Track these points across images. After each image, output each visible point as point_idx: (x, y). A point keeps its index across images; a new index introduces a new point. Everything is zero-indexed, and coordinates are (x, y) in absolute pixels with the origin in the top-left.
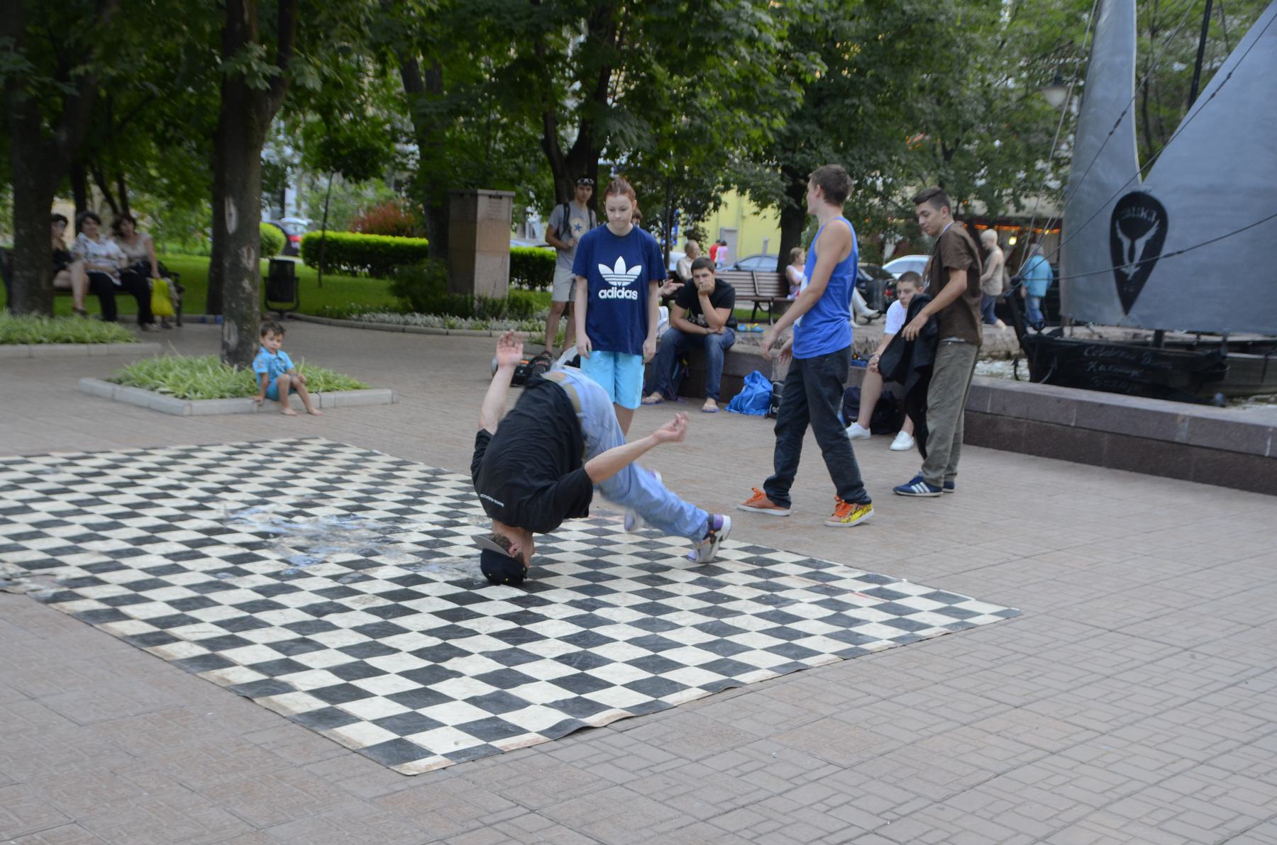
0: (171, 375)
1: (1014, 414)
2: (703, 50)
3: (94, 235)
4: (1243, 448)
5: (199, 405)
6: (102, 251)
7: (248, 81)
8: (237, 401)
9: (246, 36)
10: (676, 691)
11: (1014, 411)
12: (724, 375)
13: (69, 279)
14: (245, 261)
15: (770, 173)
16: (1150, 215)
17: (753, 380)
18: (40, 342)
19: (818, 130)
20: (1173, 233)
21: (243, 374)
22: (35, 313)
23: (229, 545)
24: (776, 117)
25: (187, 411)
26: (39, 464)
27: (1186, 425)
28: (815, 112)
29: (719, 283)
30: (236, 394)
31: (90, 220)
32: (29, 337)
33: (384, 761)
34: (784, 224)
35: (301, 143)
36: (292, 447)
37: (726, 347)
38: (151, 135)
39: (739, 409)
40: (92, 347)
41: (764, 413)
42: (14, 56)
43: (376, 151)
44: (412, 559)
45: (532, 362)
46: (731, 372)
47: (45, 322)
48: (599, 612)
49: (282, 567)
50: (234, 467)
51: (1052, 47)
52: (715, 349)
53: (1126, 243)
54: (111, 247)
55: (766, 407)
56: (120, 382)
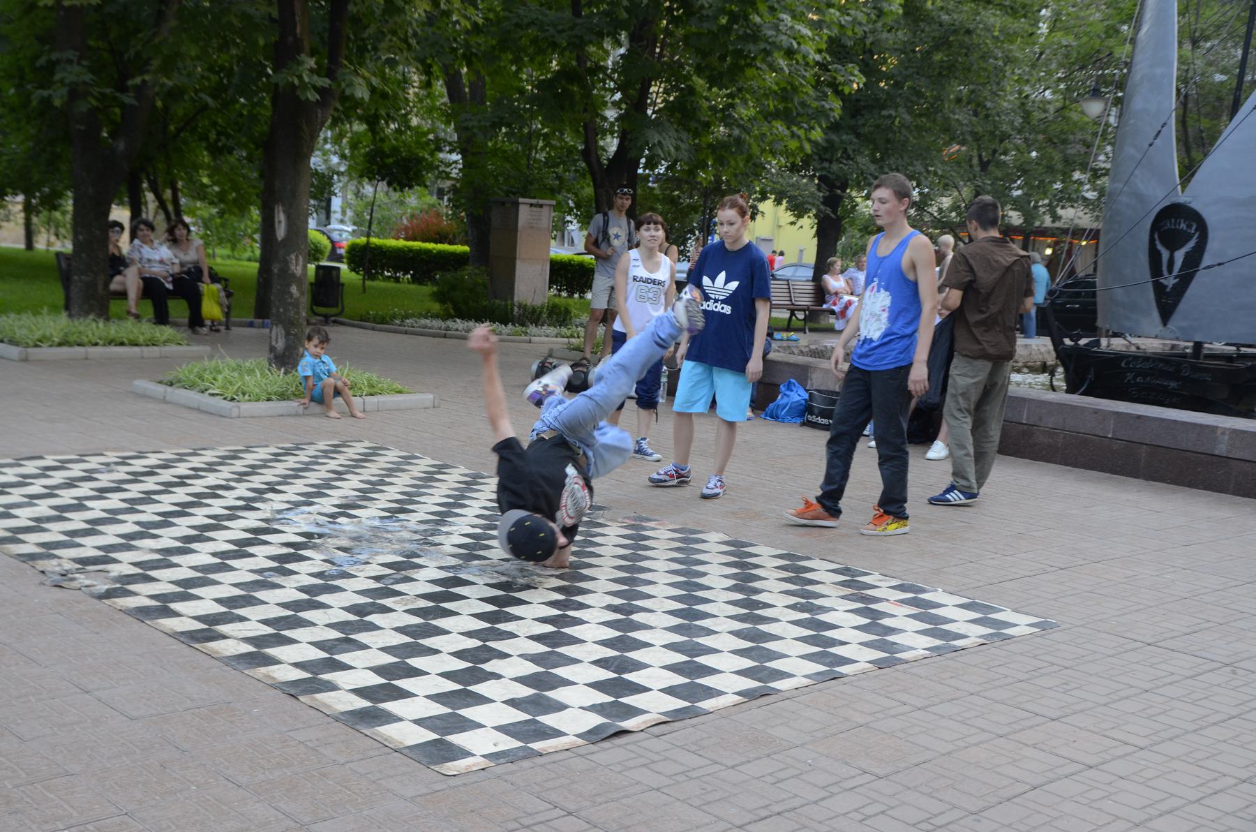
0: (220, 377)
5: (246, 407)
7: (298, 92)
11: (1050, 422)
13: (123, 284)
14: (293, 267)
15: (807, 184)
16: (1189, 226)
17: (789, 389)
18: (96, 344)
20: (1213, 245)
21: (289, 378)
22: (91, 317)
23: (275, 545)
24: (813, 128)
28: (852, 122)
30: (283, 396)
32: (86, 340)
33: (424, 761)
38: (204, 144)
39: (774, 416)
40: (145, 349)
41: (799, 421)
42: (77, 69)
44: (453, 562)
47: (101, 325)
50: (280, 468)
53: (1165, 254)
54: (165, 252)
55: (801, 415)
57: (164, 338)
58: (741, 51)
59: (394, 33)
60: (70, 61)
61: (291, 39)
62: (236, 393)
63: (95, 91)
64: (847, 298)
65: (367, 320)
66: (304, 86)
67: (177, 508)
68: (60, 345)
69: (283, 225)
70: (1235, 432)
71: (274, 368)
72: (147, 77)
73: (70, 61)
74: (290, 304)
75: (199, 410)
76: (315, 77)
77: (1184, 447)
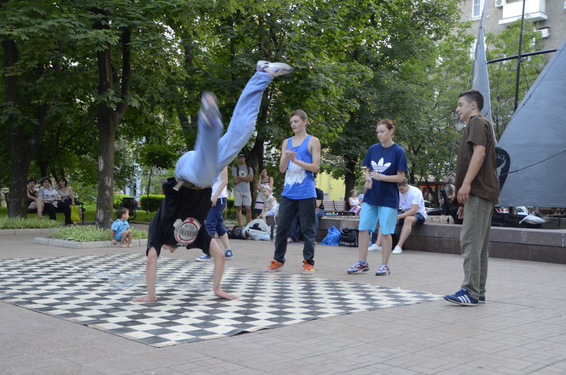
0: (74, 233)
5: (84, 244)
7: (107, 104)
8: (102, 242)
9: (108, 86)
10: (287, 321)
13: (36, 206)
16: (502, 157)
17: (332, 231)
18: (20, 228)
20: (513, 166)
21: (105, 232)
22: (18, 217)
23: (88, 282)
24: (339, 127)
26: (8, 262)
30: (102, 239)
31: (47, 181)
32: (15, 226)
34: (347, 182)
37: (320, 218)
39: (326, 243)
40: (42, 229)
41: (337, 244)
42: (13, 108)
43: (170, 156)
44: (172, 285)
45: (234, 228)
46: (322, 228)
47: (23, 220)
48: (255, 298)
49: (110, 288)
54: (55, 192)
57: (51, 225)
59: (152, 86)
60: (10, 106)
61: (105, 83)
64: (359, 207)
67: (58, 301)
68: (3, 228)
69: (102, 164)
70: (529, 232)
71: (98, 229)
72: (40, 101)
73: (10, 106)
74: (106, 199)
76: (115, 98)
77: (508, 241)
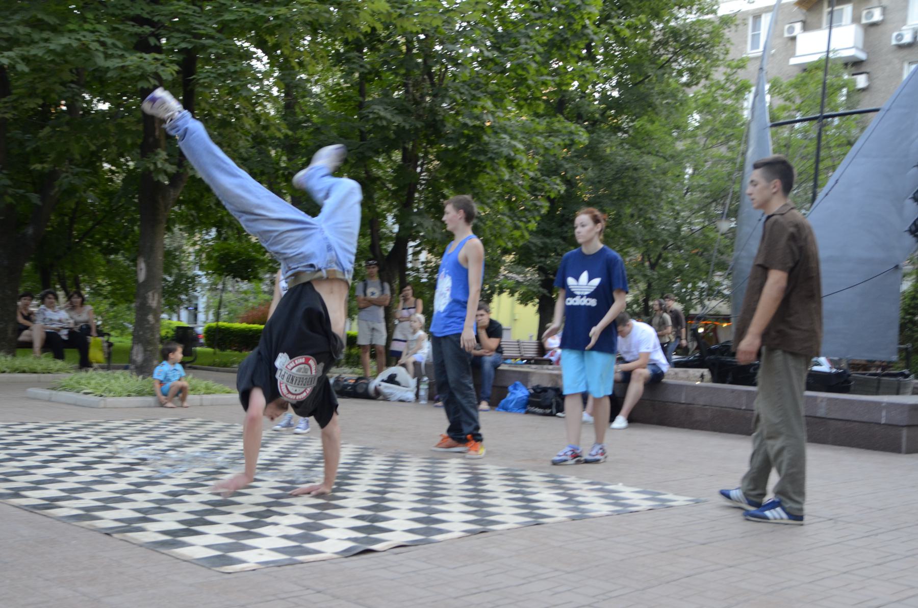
1: (702, 403)
2: (477, 169)
3: (51, 306)
4: (865, 419)
5: (111, 400)
6: (56, 317)
7: (153, 175)
11: (701, 401)
12: (494, 386)
13: (30, 336)
14: (150, 302)
15: (531, 274)
19: (562, 242)
21: (145, 382)
23: (115, 464)
24: (529, 221)
25: (102, 404)
27: (824, 404)
28: (559, 230)
29: (492, 322)
30: (140, 393)
33: (208, 565)
35: (205, 262)
36: (175, 422)
37: (495, 366)
38: (98, 248)
39: (506, 409)
41: (523, 411)
43: (255, 260)
50: (129, 430)
51: (717, 196)
52: (487, 366)
54: (63, 315)
55: (525, 408)
56: (54, 389)
57: (56, 368)
58: (476, 161)
62: (104, 391)
63: (10, 191)
65: (214, 365)
66: (158, 171)
75: (75, 405)
